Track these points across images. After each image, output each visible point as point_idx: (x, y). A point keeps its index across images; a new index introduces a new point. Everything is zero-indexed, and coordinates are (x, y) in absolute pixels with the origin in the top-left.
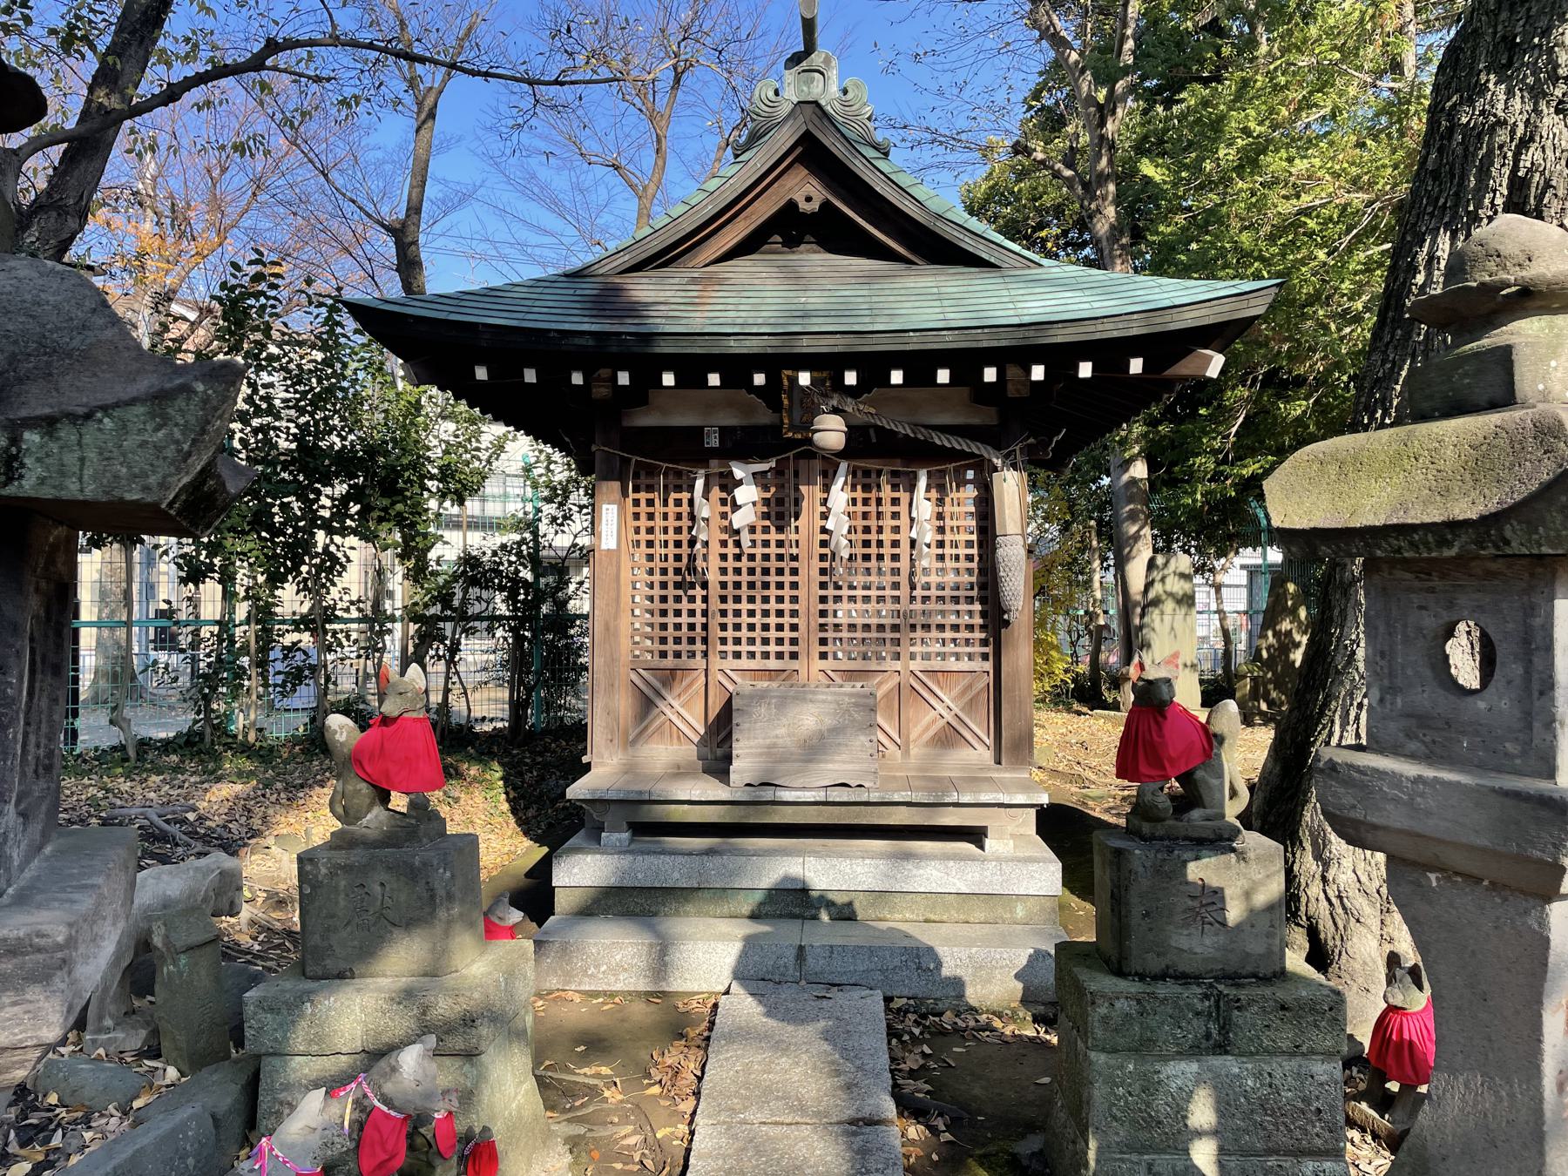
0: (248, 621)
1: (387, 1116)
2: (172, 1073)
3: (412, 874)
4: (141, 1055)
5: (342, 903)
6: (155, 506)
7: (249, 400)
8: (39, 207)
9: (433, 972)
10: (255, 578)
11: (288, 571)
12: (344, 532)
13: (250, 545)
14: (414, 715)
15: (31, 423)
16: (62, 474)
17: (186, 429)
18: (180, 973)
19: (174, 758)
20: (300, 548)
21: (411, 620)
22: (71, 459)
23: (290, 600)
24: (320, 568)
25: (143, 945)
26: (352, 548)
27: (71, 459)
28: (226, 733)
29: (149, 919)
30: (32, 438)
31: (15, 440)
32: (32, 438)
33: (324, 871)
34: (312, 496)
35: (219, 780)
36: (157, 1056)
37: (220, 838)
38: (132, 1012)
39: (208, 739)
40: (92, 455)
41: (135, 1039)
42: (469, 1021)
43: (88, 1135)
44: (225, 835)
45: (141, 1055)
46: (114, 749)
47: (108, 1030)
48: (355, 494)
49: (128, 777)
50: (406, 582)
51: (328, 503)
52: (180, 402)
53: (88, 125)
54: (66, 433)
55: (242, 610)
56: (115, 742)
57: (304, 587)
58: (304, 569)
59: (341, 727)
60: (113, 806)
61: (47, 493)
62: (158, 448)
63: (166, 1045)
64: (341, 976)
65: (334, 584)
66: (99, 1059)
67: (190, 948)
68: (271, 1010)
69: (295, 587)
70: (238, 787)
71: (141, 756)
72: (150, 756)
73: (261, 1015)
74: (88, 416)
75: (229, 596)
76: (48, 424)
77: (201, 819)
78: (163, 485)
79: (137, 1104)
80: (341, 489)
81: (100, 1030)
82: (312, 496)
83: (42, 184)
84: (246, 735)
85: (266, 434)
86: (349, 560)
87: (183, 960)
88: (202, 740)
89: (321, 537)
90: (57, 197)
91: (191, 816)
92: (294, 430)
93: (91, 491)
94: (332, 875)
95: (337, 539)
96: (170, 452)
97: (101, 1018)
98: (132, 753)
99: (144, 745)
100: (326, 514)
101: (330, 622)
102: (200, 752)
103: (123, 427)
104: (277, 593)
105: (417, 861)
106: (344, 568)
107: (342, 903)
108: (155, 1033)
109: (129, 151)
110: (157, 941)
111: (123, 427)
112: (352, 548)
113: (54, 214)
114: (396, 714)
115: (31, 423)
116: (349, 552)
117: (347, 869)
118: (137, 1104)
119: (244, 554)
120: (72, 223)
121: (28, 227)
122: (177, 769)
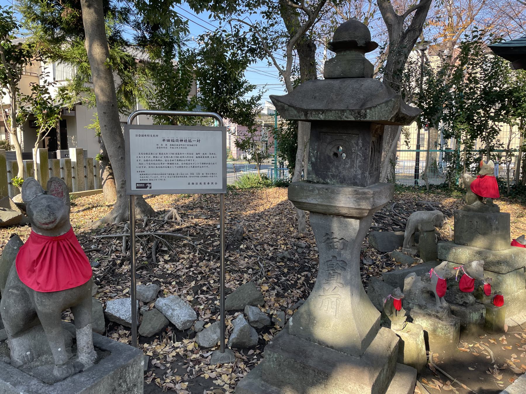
0: (464, 151)
1: (468, 277)
2: (422, 261)
3: (486, 220)
4: (415, 256)
5: (465, 225)
6: (387, 121)
7: (468, 79)
8: (408, 31)
9: (489, 248)
10: (466, 137)
11: (479, 135)
12: (499, 121)
13: (466, 126)
14: (490, 175)
15: (368, 108)
16: (373, 116)
17: (391, 107)
18: (424, 237)
19: (439, 190)
20: (482, 127)
21: (522, 151)
22: (374, 114)
23: (479, 144)
24: (489, 133)
25: (417, 230)
26: (501, 126)
27: (374, 114)
28: (455, 184)
29: (418, 223)
30: (368, 111)
31: (366, 112)
32: (368, 111)
33: (460, 216)
34: (488, 109)
35: (450, 197)
36: (419, 257)
37: (447, 213)
38: (414, 246)
39: (450, 185)
40: (377, 113)
41: (415, 252)
42: (499, 263)
43: (400, 268)
44: (449, 212)
45: (415, 256)
46: (423, 186)
47: (408, 248)
48: (503, 108)
49: (425, 193)
50: (521, 137)
51: (493, 111)
52: (390, 102)
53: (422, 2)
54: (373, 109)
55: (462, 147)
56: (423, 185)
57: (484, 139)
58: (484, 133)
59: (468, 177)
60: (419, 200)
61: (371, 120)
62: (387, 111)
63: (421, 255)
64: (464, 245)
65: (494, 138)
66: (405, 254)
67: (427, 231)
68: (445, 249)
69: (480, 140)
70: (455, 200)
71: (430, 188)
72: (433, 189)
73: (442, 250)
74: (376, 106)
75: (458, 143)
76: (370, 108)
77: (443, 207)
78: (388, 117)
79: (412, 265)
80: (498, 105)
81: (406, 247)
82: (488, 109)
83: (409, 23)
84: (461, 186)
85: (473, 89)
86: (500, 130)
87: (425, 234)
88: (448, 186)
89: (490, 122)
90: (413, 26)
91: (440, 206)
92: (483, 87)
93: (377, 119)
94: (463, 217)
95: (496, 123)
96: (389, 111)
97: (406, 245)
98: (428, 188)
99: (431, 186)
100: (492, 114)
101: (492, 151)
102: (447, 189)
103: (381, 108)
104: (474, 141)
105: (487, 217)
106: (498, 133)
107: (465, 225)
108: (419, 252)
109: (436, 6)
110: (419, 228)
111: (381, 108)
112: (501, 126)
113: (412, 32)
114: (484, 174)
115: (368, 108)
116: (500, 127)
117: (467, 216)
118: (412, 265)
119: (464, 129)
120: (417, 34)
121: (405, 37)
122: (438, 193)
